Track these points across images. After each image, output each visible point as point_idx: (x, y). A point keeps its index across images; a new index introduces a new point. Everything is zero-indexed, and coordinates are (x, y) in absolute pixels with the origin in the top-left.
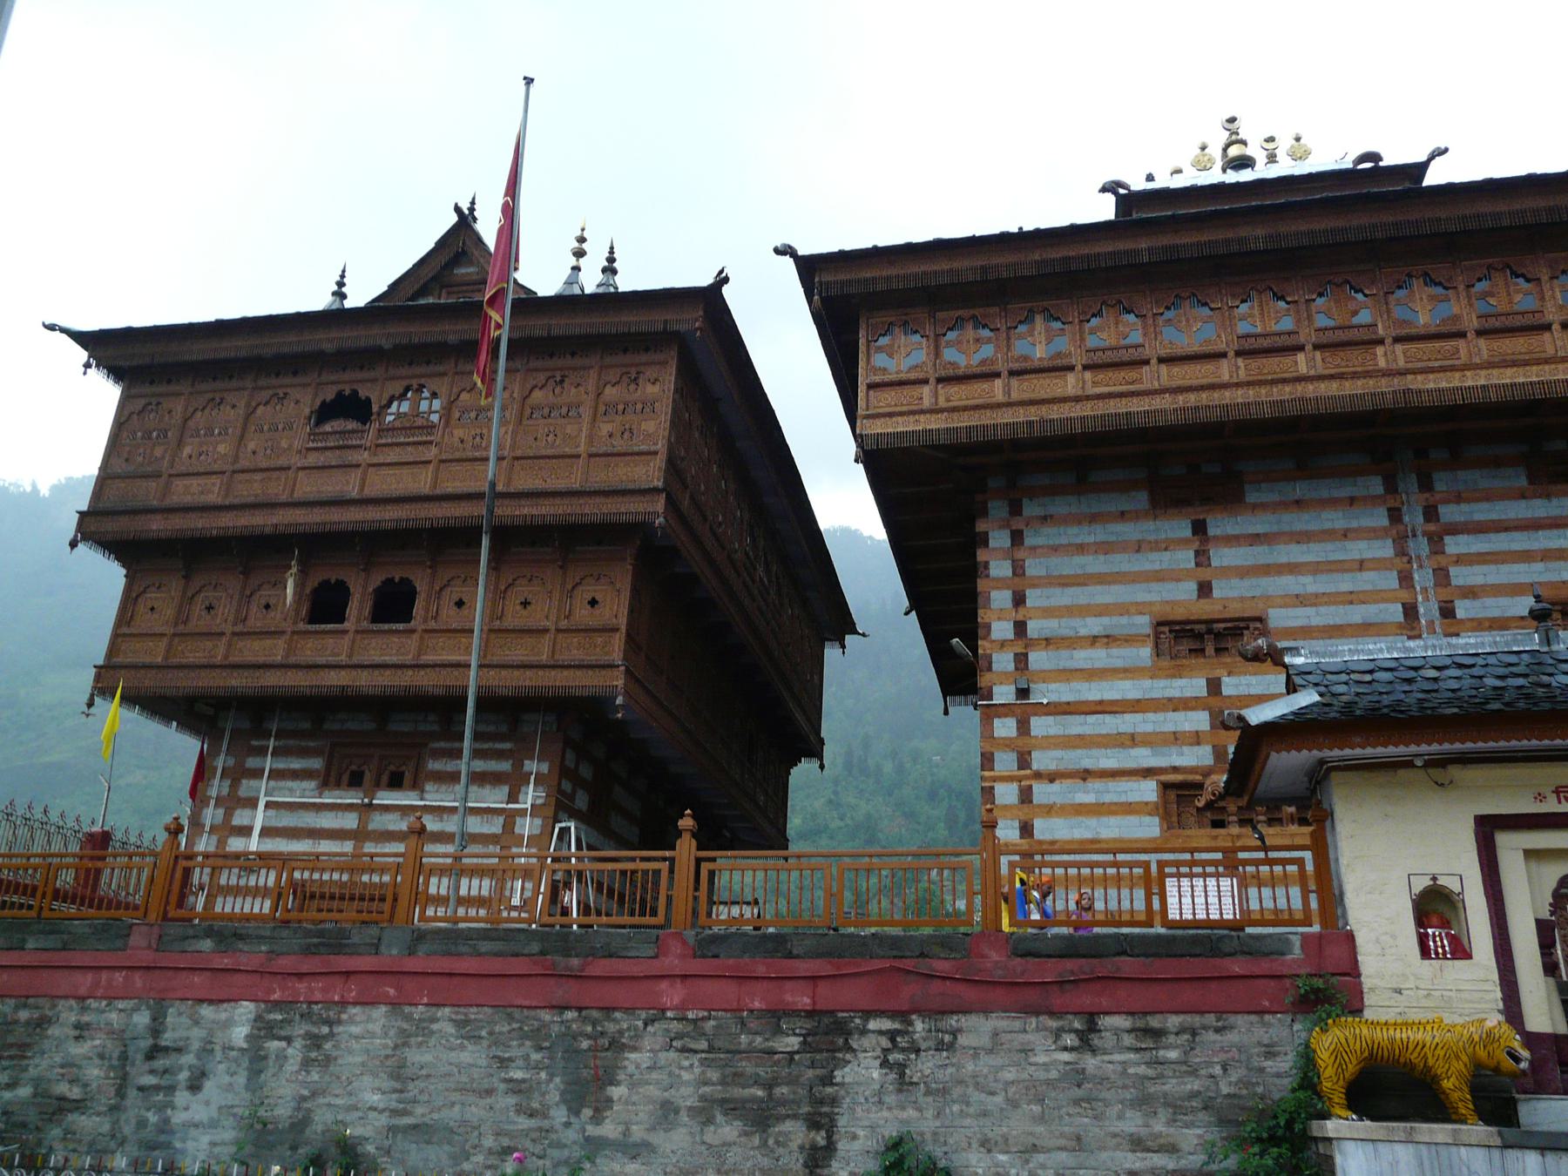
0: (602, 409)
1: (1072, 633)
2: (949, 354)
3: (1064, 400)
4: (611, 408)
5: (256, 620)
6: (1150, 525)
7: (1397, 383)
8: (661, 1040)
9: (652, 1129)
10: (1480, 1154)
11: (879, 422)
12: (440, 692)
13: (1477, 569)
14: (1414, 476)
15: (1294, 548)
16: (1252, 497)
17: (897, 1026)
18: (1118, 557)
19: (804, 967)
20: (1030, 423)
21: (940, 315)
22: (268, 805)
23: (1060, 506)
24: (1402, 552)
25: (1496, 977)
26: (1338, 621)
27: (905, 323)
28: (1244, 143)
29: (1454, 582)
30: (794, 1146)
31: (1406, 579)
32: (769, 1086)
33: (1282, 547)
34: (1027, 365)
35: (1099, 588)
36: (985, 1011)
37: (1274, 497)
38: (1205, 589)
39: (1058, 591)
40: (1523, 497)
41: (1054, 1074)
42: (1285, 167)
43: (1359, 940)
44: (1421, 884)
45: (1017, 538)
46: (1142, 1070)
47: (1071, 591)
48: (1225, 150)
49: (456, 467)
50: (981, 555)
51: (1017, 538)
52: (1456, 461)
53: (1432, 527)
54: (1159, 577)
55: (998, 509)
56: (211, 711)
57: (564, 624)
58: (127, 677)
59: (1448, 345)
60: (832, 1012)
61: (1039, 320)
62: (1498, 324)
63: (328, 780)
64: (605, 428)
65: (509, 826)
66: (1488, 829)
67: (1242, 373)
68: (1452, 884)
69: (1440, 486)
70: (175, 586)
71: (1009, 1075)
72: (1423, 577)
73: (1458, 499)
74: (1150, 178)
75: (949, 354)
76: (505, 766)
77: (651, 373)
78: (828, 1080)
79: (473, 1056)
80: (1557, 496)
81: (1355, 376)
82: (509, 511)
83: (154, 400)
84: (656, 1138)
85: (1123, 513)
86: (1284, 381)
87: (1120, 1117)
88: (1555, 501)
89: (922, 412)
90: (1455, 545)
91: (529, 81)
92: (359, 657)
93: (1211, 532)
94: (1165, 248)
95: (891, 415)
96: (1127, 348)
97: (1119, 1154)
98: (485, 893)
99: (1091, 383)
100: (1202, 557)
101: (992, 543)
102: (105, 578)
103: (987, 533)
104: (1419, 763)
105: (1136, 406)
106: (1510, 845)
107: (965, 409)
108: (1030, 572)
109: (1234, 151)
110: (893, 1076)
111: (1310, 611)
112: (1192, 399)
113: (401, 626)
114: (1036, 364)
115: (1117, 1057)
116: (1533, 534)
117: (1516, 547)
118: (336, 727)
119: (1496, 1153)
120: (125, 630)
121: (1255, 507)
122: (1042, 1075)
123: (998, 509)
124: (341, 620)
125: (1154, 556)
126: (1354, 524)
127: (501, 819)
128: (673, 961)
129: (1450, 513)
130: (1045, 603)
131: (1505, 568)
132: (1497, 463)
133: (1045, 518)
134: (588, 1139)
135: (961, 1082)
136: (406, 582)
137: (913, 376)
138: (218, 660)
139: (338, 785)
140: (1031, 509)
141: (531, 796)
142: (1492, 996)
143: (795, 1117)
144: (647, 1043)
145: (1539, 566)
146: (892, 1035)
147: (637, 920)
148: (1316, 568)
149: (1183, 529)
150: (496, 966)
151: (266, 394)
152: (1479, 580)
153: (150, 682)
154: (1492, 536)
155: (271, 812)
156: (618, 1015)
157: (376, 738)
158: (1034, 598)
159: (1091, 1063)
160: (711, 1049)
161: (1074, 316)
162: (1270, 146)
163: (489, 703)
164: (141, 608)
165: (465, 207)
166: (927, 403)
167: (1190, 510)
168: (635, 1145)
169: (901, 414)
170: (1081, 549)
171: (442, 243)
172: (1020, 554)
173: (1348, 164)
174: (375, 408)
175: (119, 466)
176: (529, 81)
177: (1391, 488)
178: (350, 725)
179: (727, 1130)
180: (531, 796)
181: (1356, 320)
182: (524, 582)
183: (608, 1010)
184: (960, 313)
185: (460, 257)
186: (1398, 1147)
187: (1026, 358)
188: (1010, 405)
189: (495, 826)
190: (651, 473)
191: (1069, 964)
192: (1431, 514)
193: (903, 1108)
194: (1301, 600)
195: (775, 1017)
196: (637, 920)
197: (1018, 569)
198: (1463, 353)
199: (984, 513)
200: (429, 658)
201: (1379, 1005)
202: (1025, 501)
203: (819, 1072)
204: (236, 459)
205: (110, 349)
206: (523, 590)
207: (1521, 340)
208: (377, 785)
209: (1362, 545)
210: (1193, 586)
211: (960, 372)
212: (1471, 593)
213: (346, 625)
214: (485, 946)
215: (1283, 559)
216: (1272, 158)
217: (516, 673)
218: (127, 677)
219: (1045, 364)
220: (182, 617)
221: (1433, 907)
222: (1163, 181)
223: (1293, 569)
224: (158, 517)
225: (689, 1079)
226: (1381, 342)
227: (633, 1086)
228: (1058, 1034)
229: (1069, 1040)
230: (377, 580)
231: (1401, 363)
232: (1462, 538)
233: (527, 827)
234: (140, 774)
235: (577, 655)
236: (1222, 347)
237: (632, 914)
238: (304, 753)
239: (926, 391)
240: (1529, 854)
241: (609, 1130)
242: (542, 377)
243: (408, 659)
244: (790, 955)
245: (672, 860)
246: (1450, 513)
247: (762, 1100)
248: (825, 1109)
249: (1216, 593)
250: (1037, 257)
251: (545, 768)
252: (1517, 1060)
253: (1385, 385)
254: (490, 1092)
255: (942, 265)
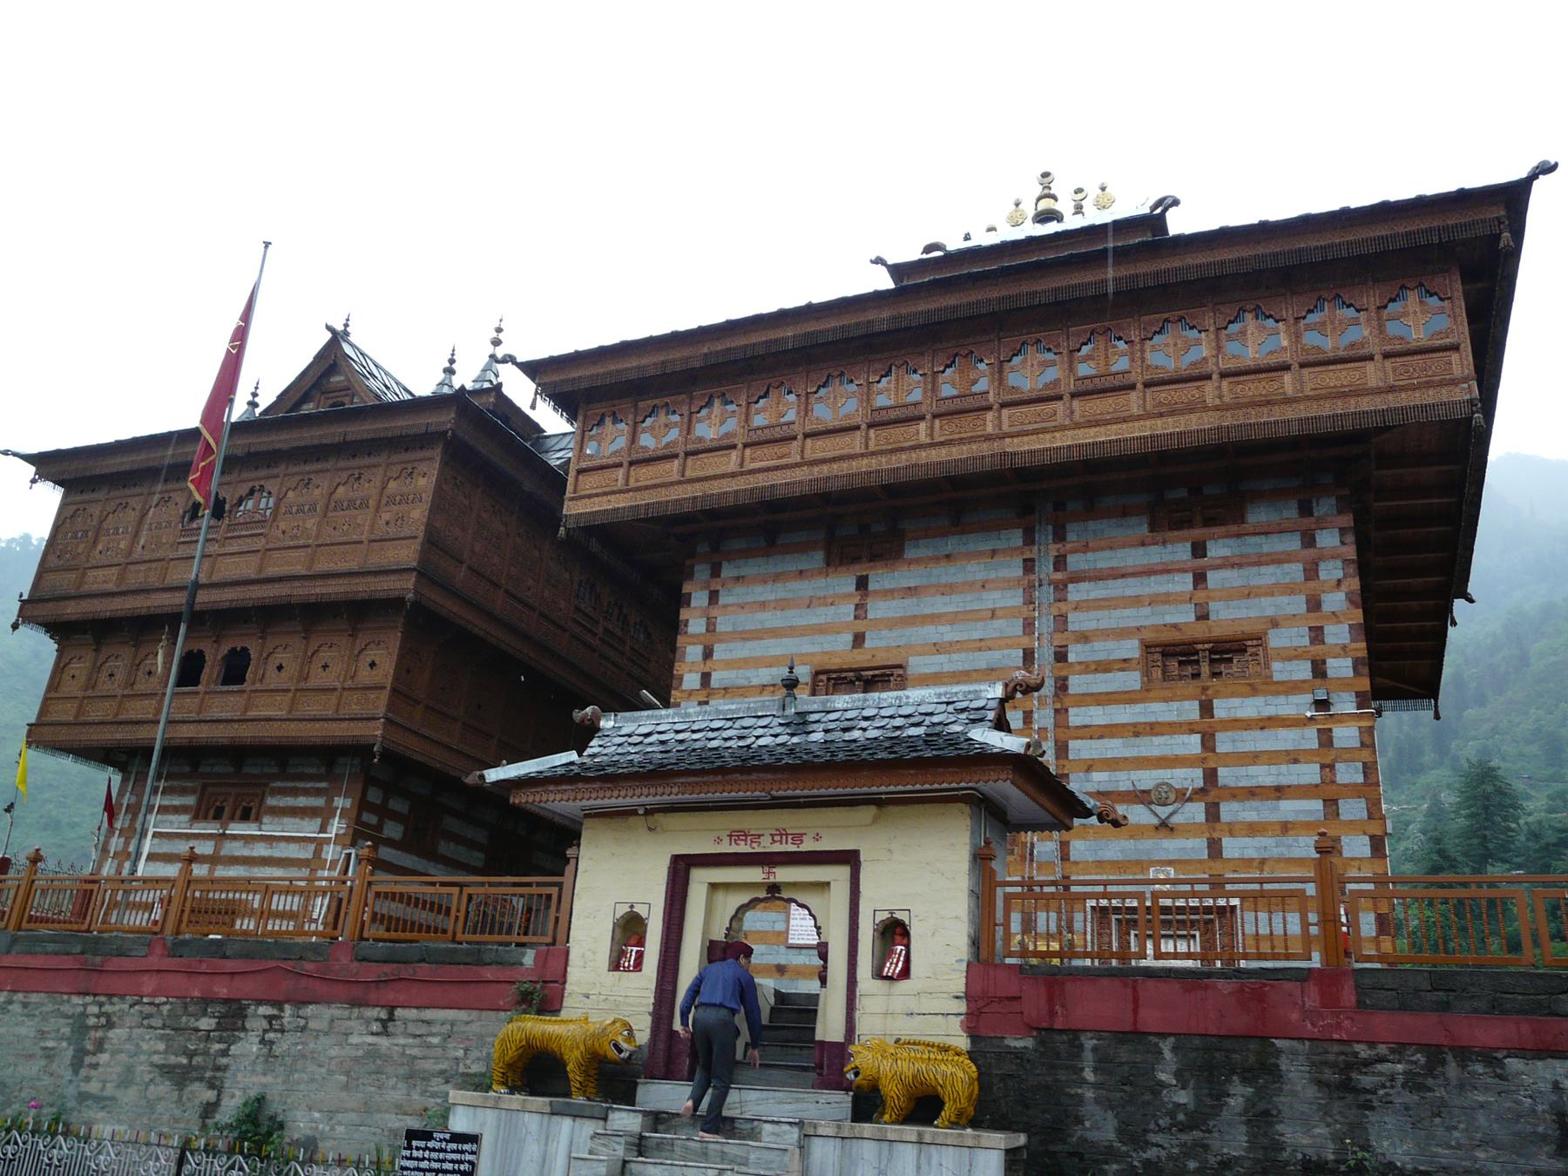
0: (384, 502)
1: (745, 683)
2: (1311, 339)
3: (723, 476)
4: (391, 501)
5: (140, 687)
6: (820, 582)
7: (997, 447)
8: (137, 1019)
9: (118, 1087)
10: (536, 1117)
11: (579, 503)
12: (226, 742)
13: (1093, 614)
14: (1050, 528)
15: (939, 599)
16: (910, 553)
17: (275, 1012)
18: (791, 613)
19: (229, 965)
20: (695, 498)
21: (641, 404)
22: (155, 835)
23: (751, 568)
24: (1029, 601)
25: (653, 986)
26: (967, 667)
27: (842, 374)
28: (1055, 198)
29: (1071, 627)
30: (197, 1102)
31: (1029, 626)
32: (191, 1055)
33: (929, 598)
34: (700, 446)
35: (773, 641)
36: (327, 1001)
37: (930, 553)
38: (859, 640)
39: (739, 644)
40: (1143, 544)
41: (360, 1053)
42: (1094, 217)
43: (572, 956)
44: (623, 910)
45: (714, 597)
46: (415, 1051)
47: (749, 644)
48: (1039, 199)
49: (276, 554)
50: (684, 614)
51: (714, 597)
52: (1091, 512)
53: (1059, 576)
54: (821, 630)
55: (702, 571)
56: (123, 758)
57: (349, 683)
58: (42, 735)
59: (1048, 407)
60: (238, 1000)
61: (1249, 316)
62: (1117, 383)
63: (198, 815)
64: (386, 517)
65: (318, 853)
66: (681, 869)
67: (872, 444)
68: (641, 910)
69: (1071, 536)
70: (127, 652)
71: (333, 1052)
72: (1044, 625)
73: (1086, 549)
74: (967, 238)
75: (1013, 379)
76: (319, 802)
77: (423, 467)
78: (225, 1053)
79: (27, 1029)
80: (1172, 541)
81: (961, 441)
82: (203, 597)
83: (81, 506)
84: (119, 1094)
85: (801, 572)
86: (902, 449)
87: (394, 1088)
88: (1169, 547)
89: (613, 493)
90: (1076, 592)
91: (267, 244)
92: (221, 714)
93: (872, 586)
94: (806, 335)
95: (589, 496)
96: (781, 425)
97: (387, 1116)
98: (295, 908)
99: (942, 429)
100: (1200, 579)
101: (693, 604)
102: (40, 649)
103: (690, 594)
104: (641, 812)
105: (779, 478)
106: (700, 879)
107: (647, 488)
108: (720, 628)
109: (1045, 204)
110: (265, 1051)
111: (942, 658)
112: (825, 470)
113: (235, 688)
114: (708, 444)
115: (402, 1041)
116: (1145, 580)
117: (1129, 592)
118: (208, 769)
119: (546, 1117)
120: (53, 695)
121: (910, 562)
122: (353, 1053)
123: (702, 571)
124: (196, 683)
125: (822, 610)
126: (993, 575)
127: (313, 846)
128: (155, 961)
129: (1076, 562)
130: (728, 656)
131: (1117, 613)
132: (1124, 513)
133: (738, 578)
134: (80, 1094)
135: (304, 1056)
136: (245, 650)
137: (610, 461)
138: (109, 718)
139: (205, 818)
140: (728, 571)
141: (336, 826)
142: (644, 1001)
143: (201, 1079)
144: (128, 1021)
145: (1147, 611)
146: (270, 1018)
147: (393, 935)
148: (954, 618)
149: (1181, 552)
150: (53, 962)
151: (113, 504)
152: (1092, 625)
153: (64, 735)
154: (1110, 582)
155: (156, 841)
156: (115, 1000)
157: (228, 777)
158: (720, 652)
159: (383, 1042)
160: (164, 1027)
161: (1134, 335)
162: (1080, 196)
163: (172, 752)
164: (66, 677)
165: (340, 328)
166: (620, 484)
167: (857, 567)
168: (106, 1098)
169: (597, 495)
170: (763, 605)
171: (320, 357)
172: (714, 612)
173: (1145, 210)
174: (227, 507)
175: (53, 561)
176: (267, 244)
177: (1029, 540)
178: (216, 769)
179: (164, 1088)
180: (336, 826)
181: (976, 389)
182: (372, 646)
183: (110, 996)
184: (656, 401)
185: (333, 369)
186: (489, 1111)
187: (700, 440)
188: (932, 445)
189: (306, 853)
190: (407, 554)
191: (387, 968)
192: (1060, 563)
193: (265, 1074)
194: (938, 648)
195: (206, 1002)
196: (393, 935)
197: (711, 627)
198: (1060, 414)
199: (690, 576)
200: (252, 714)
201: (573, 1005)
202: (725, 564)
203: (222, 1046)
204: (130, 553)
205: (48, 465)
206: (325, 655)
207: (1110, 400)
208: (232, 819)
209: (996, 595)
210: (849, 638)
211: (647, 455)
212: (1084, 638)
213: (200, 688)
214: (51, 947)
215: (928, 611)
216: (1079, 209)
217: (310, 725)
218: (42, 735)
219: (715, 444)
220: (91, 684)
221: (630, 928)
222: (984, 239)
223: (934, 619)
224: (73, 603)
225: (153, 1046)
226: (990, 408)
227: (113, 1054)
228: (368, 1022)
229: (375, 1027)
230: (225, 649)
231: (1005, 428)
232: (1084, 586)
233: (330, 853)
234: (61, 812)
235: (356, 709)
236: (1286, 357)
237: (388, 930)
238: (183, 792)
239: (621, 472)
240: (714, 887)
241: (93, 1087)
242: (345, 475)
243: (237, 715)
244: (225, 957)
245: (560, 885)
246: (1076, 562)
247: (184, 1066)
248: (219, 1074)
249: (868, 644)
250: (705, 350)
251: (348, 803)
252: (620, 1051)
253: (985, 449)
254: (31, 1056)
255: (1227, 255)
